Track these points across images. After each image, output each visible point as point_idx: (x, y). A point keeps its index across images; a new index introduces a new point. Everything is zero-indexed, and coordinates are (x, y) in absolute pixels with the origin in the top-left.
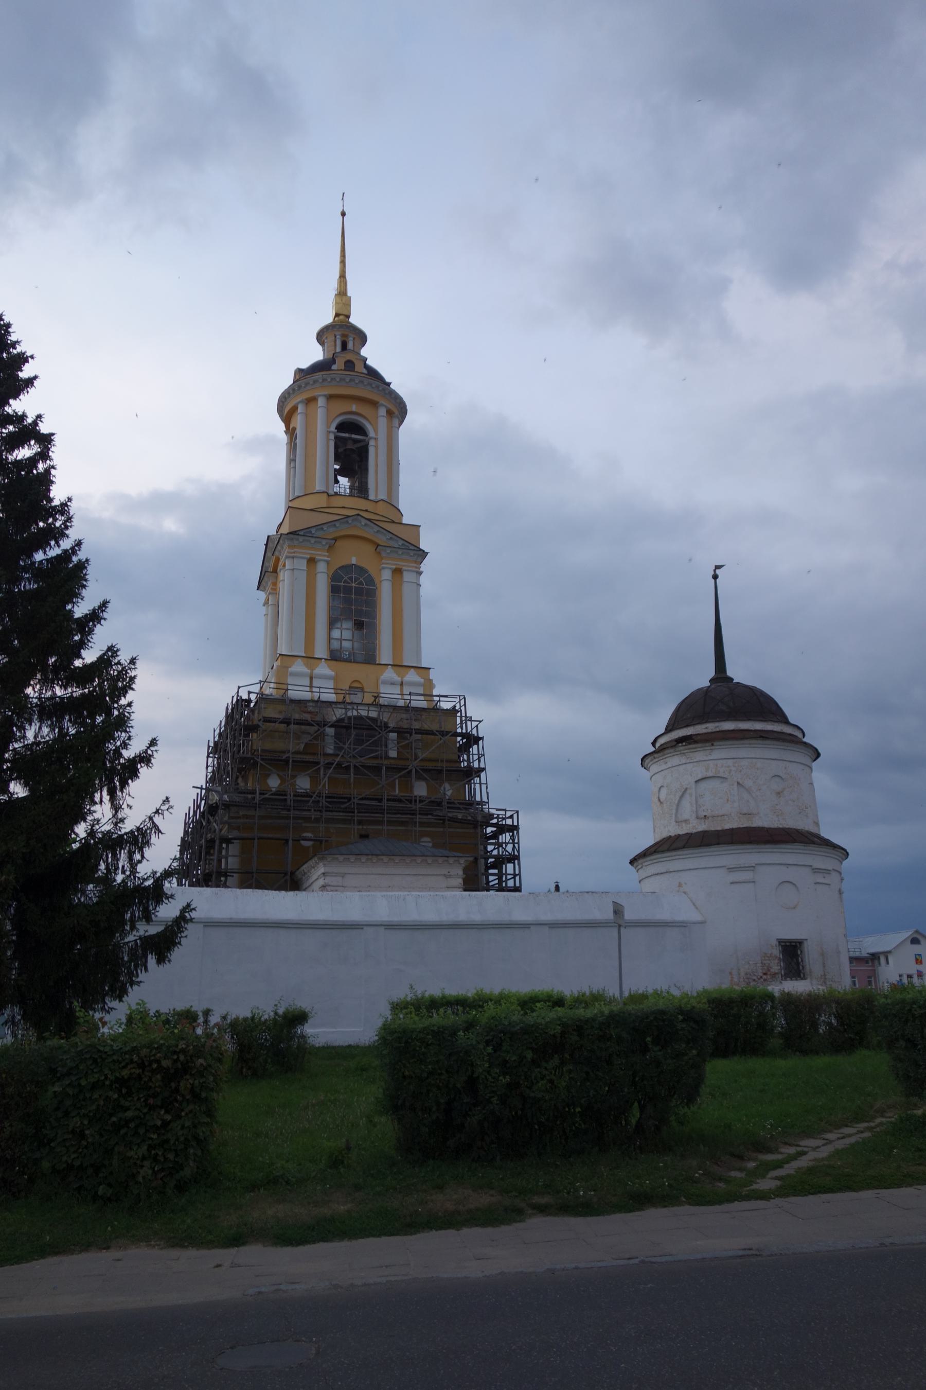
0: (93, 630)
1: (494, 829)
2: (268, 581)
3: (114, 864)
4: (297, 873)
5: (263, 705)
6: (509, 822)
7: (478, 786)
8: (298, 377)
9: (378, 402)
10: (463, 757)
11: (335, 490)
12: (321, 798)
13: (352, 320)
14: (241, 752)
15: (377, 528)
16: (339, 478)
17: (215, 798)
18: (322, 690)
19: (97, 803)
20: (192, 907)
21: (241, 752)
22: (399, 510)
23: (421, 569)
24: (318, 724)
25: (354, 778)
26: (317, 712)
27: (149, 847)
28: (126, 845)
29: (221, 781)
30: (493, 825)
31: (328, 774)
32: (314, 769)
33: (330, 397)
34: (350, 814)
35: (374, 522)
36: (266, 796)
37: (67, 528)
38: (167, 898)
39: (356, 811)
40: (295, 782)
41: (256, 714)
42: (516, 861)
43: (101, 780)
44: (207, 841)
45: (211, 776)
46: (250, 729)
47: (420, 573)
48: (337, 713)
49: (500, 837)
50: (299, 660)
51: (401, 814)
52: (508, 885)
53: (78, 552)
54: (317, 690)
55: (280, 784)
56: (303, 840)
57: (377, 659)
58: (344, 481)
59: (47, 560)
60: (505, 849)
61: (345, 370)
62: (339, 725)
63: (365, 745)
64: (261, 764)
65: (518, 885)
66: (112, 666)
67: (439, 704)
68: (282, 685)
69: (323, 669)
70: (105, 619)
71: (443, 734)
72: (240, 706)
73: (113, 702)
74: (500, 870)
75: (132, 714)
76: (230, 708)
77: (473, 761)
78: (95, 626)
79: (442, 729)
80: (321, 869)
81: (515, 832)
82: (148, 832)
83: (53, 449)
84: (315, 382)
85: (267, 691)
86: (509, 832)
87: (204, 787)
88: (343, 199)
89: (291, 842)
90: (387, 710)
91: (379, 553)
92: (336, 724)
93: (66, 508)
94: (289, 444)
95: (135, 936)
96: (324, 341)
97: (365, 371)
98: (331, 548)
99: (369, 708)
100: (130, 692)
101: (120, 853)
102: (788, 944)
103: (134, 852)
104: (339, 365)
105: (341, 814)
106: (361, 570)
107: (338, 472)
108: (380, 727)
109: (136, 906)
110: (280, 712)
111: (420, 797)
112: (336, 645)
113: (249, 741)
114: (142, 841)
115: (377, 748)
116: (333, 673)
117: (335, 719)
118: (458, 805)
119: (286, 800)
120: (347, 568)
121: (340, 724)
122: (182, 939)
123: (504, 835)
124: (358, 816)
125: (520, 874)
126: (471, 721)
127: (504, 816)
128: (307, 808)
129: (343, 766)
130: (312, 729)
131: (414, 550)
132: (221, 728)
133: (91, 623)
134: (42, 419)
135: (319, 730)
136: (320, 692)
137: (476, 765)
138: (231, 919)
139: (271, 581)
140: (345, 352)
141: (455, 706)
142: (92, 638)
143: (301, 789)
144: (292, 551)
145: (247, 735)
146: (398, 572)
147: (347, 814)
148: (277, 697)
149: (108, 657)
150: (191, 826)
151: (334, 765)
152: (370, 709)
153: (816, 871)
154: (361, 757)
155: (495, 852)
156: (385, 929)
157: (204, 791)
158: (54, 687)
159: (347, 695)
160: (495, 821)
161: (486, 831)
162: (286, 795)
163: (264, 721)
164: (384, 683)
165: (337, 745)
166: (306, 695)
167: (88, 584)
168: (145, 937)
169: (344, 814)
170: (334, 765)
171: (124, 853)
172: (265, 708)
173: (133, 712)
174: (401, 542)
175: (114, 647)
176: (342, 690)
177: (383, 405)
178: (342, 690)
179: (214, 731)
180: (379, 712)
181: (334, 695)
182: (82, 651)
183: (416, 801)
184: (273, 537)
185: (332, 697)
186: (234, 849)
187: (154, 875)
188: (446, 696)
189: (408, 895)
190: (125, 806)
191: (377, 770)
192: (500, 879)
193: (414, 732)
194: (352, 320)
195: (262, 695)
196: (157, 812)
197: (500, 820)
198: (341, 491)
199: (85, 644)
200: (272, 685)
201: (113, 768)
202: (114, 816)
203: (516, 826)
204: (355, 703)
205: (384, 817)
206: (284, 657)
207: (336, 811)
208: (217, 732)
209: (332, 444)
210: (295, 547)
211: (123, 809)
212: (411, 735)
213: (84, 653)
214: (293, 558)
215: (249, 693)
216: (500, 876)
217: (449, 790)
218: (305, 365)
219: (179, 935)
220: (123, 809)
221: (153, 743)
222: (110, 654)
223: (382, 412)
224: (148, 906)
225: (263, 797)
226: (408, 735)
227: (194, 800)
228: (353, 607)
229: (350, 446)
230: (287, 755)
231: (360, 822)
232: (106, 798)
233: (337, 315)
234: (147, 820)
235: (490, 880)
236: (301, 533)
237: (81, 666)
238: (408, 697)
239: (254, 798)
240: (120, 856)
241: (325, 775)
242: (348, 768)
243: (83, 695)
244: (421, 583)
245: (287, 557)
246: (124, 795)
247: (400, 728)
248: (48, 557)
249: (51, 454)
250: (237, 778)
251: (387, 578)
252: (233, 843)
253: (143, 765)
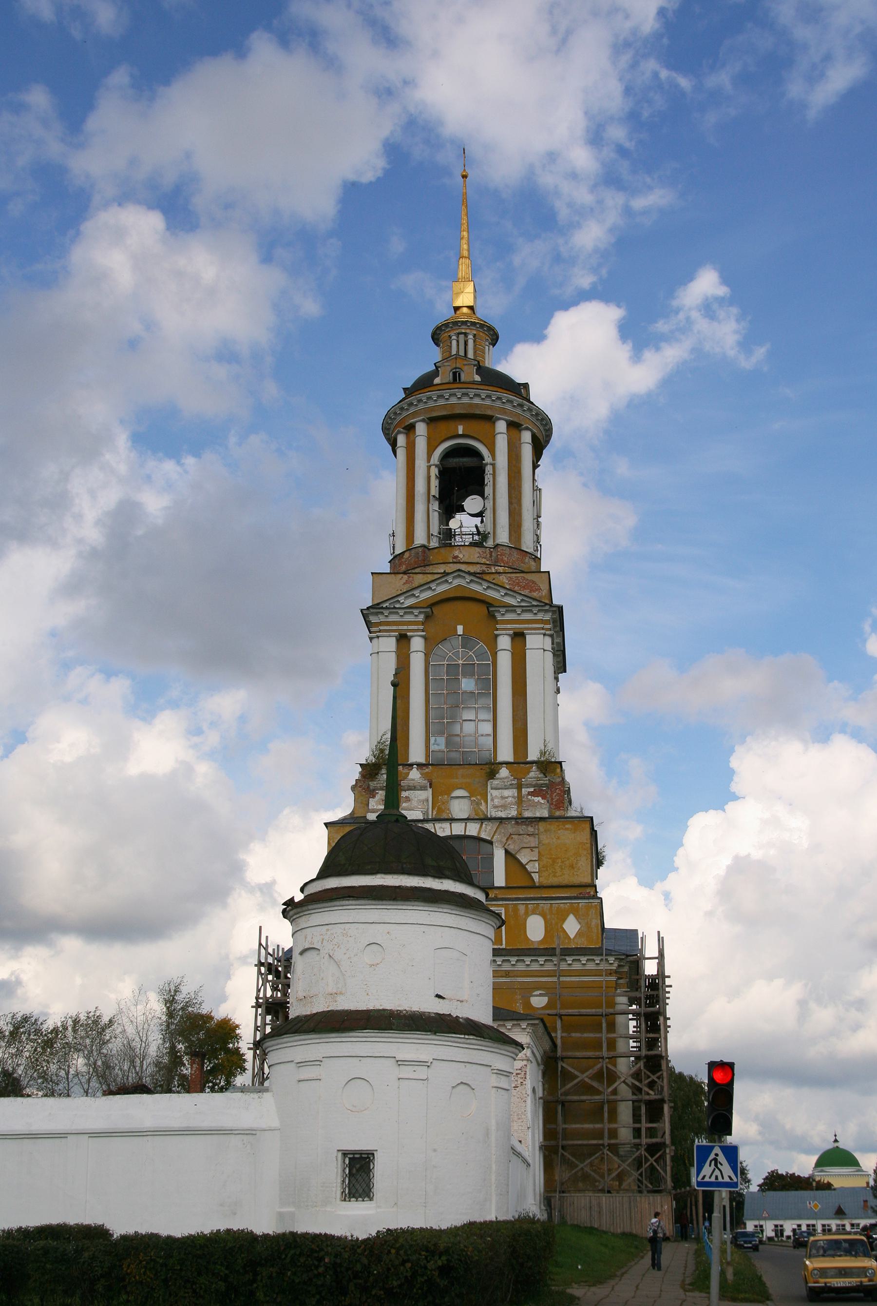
9: (493, 416)
35: (477, 575)
102: (357, 1156)
153: (400, 1063)
236: (387, 604)
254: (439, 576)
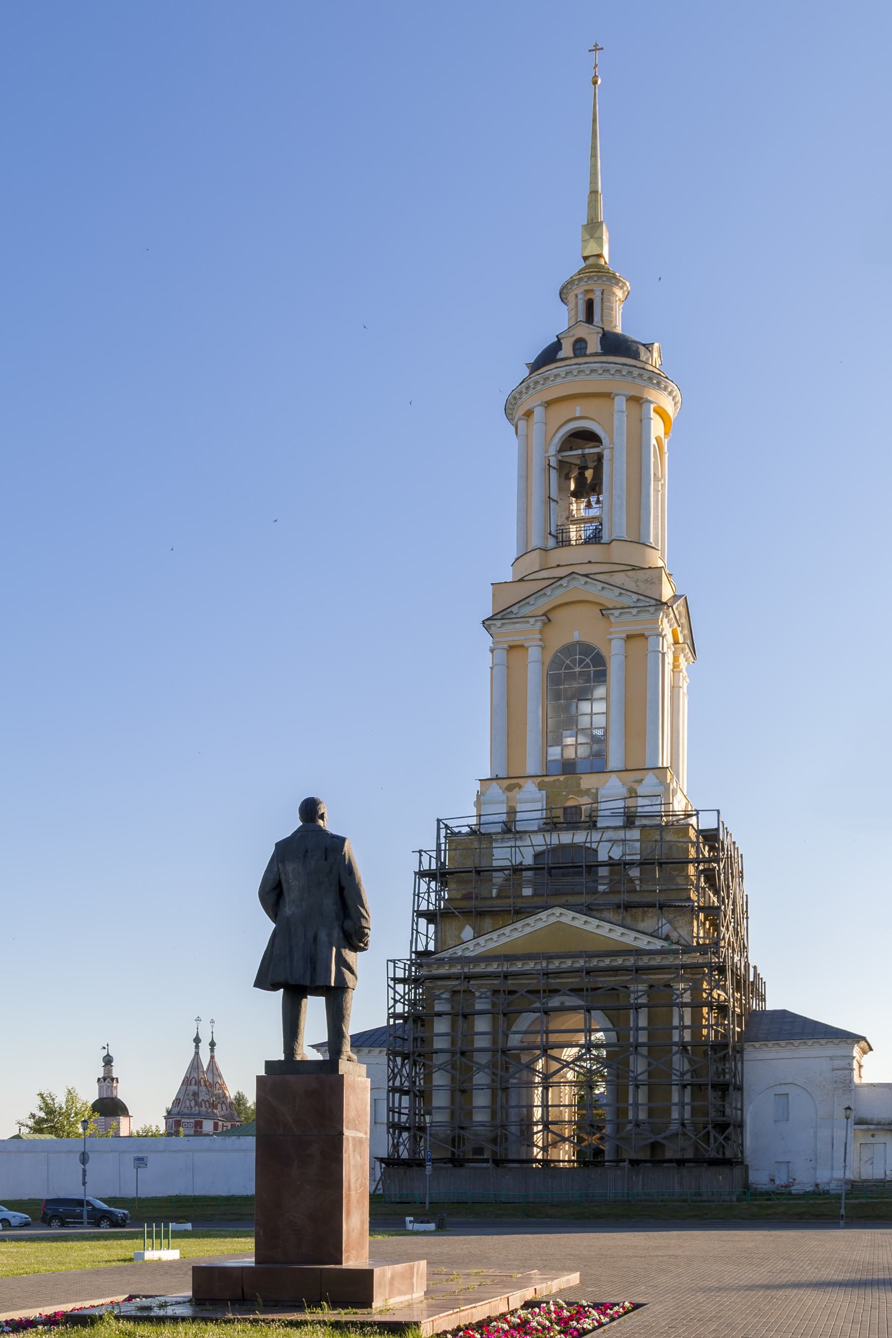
15: (600, 585)
25: (845, 1203)
43: (330, 935)
174: (635, 597)
254: (556, 580)
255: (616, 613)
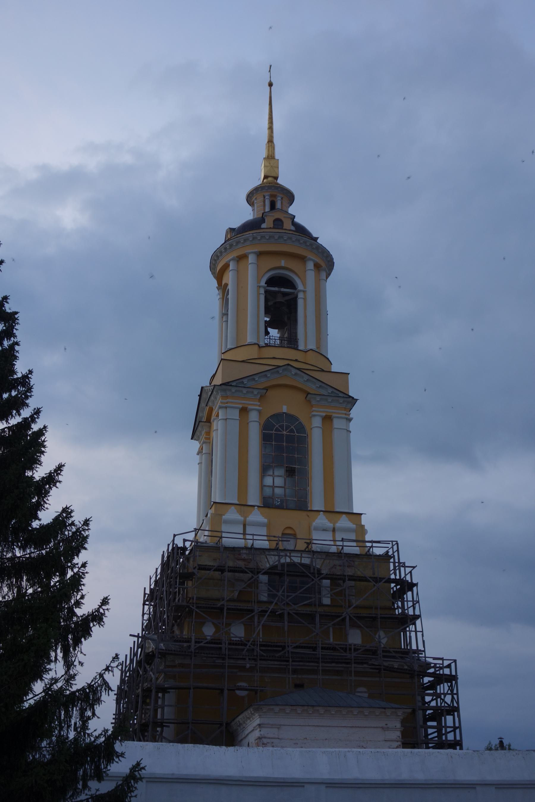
0: (49, 492)
1: (431, 679)
2: (202, 431)
3: (67, 721)
4: (233, 723)
5: (198, 553)
6: (447, 671)
7: (413, 634)
8: (229, 236)
10: (397, 604)
11: (266, 342)
12: (256, 646)
13: (280, 181)
14: (177, 599)
15: (306, 377)
16: (269, 329)
17: (151, 646)
18: (255, 537)
19: (52, 661)
20: (141, 766)
21: (177, 599)
22: (328, 359)
23: (351, 416)
24: (252, 572)
26: (251, 560)
27: (99, 704)
28: (78, 703)
29: (157, 628)
30: (430, 675)
31: (262, 622)
32: (248, 616)
33: (260, 254)
34: (285, 663)
35: (301, 370)
36: (202, 644)
37: (27, 397)
38: (118, 757)
39: (291, 660)
40: (230, 629)
41: (191, 562)
42: (456, 713)
44: (143, 691)
45: (147, 624)
46: (186, 577)
47: (350, 420)
48: (270, 560)
49: (438, 687)
50: (233, 508)
51: (337, 663)
52: (448, 739)
53: (37, 420)
54: (251, 537)
55: (215, 632)
56: (239, 689)
57: (309, 505)
58: (274, 333)
59: (9, 428)
60: (443, 700)
61: (274, 228)
62: (272, 572)
63: (299, 592)
64: (196, 611)
65: (458, 738)
66: (66, 526)
67: (371, 550)
68: (216, 533)
69: (256, 516)
70: (60, 482)
71: (377, 580)
72: (175, 554)
73: (67, 562)
74: (440, 723)
75: (86, 574)
76: (166, 555)
77: (408, 608)
78: (51, 488)
79: (375, 576)
80: (257, 721)
81: (454, 682)
82: (99, 689)
83: (17, 327)
84: (245, 240)
85: (202, 539)
86: (447, 682)
87: (140, 635)
88: (270, 71)
89: (226, 692)
90: (320, 557)
91: (309, 401)
92: (270, 571)
93: (27, 380)
94: (221, 300)
95: (87, 795)
96: (253, 202)
97: (293, 228)
98: (262, 398)
99: (301, 554)
100: (83, 551)
101: (73, 710)
103: (86, 710)
104: (268, 223)
105: (276, 663)
106: (291, 418)
107: (268, 325)
108: (313, 574)
109: (88, 764)
110: (215, 560)
111: (355, 645)
112: (268, 492)
113: (185, 588)
114: (93, 698)
115: (311, 596)
116: (266, 520)
117: (268, 566)
118: (394, 654)
119: (221, 648)
120: (278, 417)
121: (273, 571)
122: (131, 798)
123: (442, 685)
124: (292, 665)
125: (460, 727)
126: (405, 567)
127: (441, 666)
128: (241, 657)
129: (277, 613)
130: (246, 577)
131: (343, 397)
132: (156, 576)
133: (47, 486)
134: (8, 301)
135: (252, 577)
136: (253, 540)
137: (411, 612)
138: (173, 774)
139: (204, 431)
140: (273, 211)
141: (388, 552)
142: (47, 500)
143: (236, 637)
144: (225, 401)
145: (182, 583)
146: (328, 419)
147: (282, 663)
148: (211, 544)
149: (63, 518)
150: (128, 675)
151: (268, 613)
152: (303, 555)
154: (295, 604)
155: (433, 704)
156: (326, 787)
157: (140, 639)
158: (14, 549)
159: (280, 542)
160: (432, 670)
161: (423, 681)
162: (221, 643)
163: (199, 569)
164: (316, 529)
165: (271, 593)
166: (240, 543)
167: (46, 450)
168: (96, 796)
169: (279, 663)
170: (268, 613)
171: (77, 710)
172: (199, 556)
173: (87, 573)
174: (330, 390)
175: (68, 508)
176: (274, 537)
177: (310, 259)
178: (274, 537)
179: (150, 579)
180: (312, 558)
181: (267, 542)
182: (39, 512)
183: (350, 649)
184: (206, 388)
185: (265, 544)
186: (170, 698)
187: (105, 733)
188: (379, 542)
189: (349, 751)
190: (76, 663)
191: (311, 617)
192: (439, 731)
193: (347, 578)
194: (281, 181)
195: (197, 543)
196: (107, 669)
197: (437, 669)
198: (271, 342)
199: (42, 505)
200: (206, 533)
201: (67, 627)
202: (66, 673)
203: (454, 676)
204: (288, 550)
205: (318, 667)
206: (218, 505)
207: (271, 660)
208: (153, 579)
209: (262, 298)
210: (227, 397)
211: (75, 666)
212: (344, 581)
213: (40, 514)
214: (226, 408)
215: (185, 541)
216: (439, 729)
217: (384, 638)
218: (236, 224)
219: (129, 795)
220: (75, 666)
221: (105, 601)
222: (64, 515)
223: (310, 265)
224: (100, 765)
225: (198, 645)
226: (341, 582)
227: (131, 648)
228: (285, 455)
229: (280, 299)
230: (222, 603)
231: (295, 672)
232: (60, 655)
233: (266, 177)
234: (98, 677)
235: (429, 732)
236: (234, 384)
237: (38, 527)
238: (340, 543)
239: (189, 647)
240: (73, 713)
241: (259, 622)
242: (281, 616)
243: (40, 556)
244: (351, 430)
245: (220, 407)
246: (76, 652)
247: (333, 575)
248: (10, 425)
249: (15, 331)
250: (173, 625)
251: (318, 426)
252: (169, 692)
253: (95, 624)
255: (318, 398)
